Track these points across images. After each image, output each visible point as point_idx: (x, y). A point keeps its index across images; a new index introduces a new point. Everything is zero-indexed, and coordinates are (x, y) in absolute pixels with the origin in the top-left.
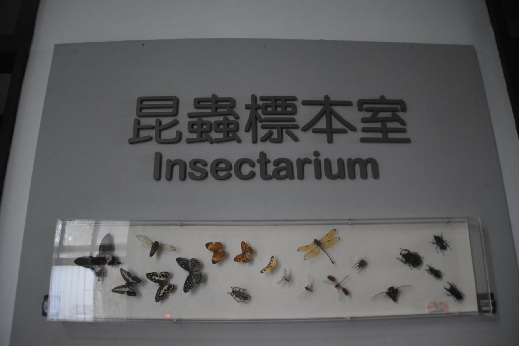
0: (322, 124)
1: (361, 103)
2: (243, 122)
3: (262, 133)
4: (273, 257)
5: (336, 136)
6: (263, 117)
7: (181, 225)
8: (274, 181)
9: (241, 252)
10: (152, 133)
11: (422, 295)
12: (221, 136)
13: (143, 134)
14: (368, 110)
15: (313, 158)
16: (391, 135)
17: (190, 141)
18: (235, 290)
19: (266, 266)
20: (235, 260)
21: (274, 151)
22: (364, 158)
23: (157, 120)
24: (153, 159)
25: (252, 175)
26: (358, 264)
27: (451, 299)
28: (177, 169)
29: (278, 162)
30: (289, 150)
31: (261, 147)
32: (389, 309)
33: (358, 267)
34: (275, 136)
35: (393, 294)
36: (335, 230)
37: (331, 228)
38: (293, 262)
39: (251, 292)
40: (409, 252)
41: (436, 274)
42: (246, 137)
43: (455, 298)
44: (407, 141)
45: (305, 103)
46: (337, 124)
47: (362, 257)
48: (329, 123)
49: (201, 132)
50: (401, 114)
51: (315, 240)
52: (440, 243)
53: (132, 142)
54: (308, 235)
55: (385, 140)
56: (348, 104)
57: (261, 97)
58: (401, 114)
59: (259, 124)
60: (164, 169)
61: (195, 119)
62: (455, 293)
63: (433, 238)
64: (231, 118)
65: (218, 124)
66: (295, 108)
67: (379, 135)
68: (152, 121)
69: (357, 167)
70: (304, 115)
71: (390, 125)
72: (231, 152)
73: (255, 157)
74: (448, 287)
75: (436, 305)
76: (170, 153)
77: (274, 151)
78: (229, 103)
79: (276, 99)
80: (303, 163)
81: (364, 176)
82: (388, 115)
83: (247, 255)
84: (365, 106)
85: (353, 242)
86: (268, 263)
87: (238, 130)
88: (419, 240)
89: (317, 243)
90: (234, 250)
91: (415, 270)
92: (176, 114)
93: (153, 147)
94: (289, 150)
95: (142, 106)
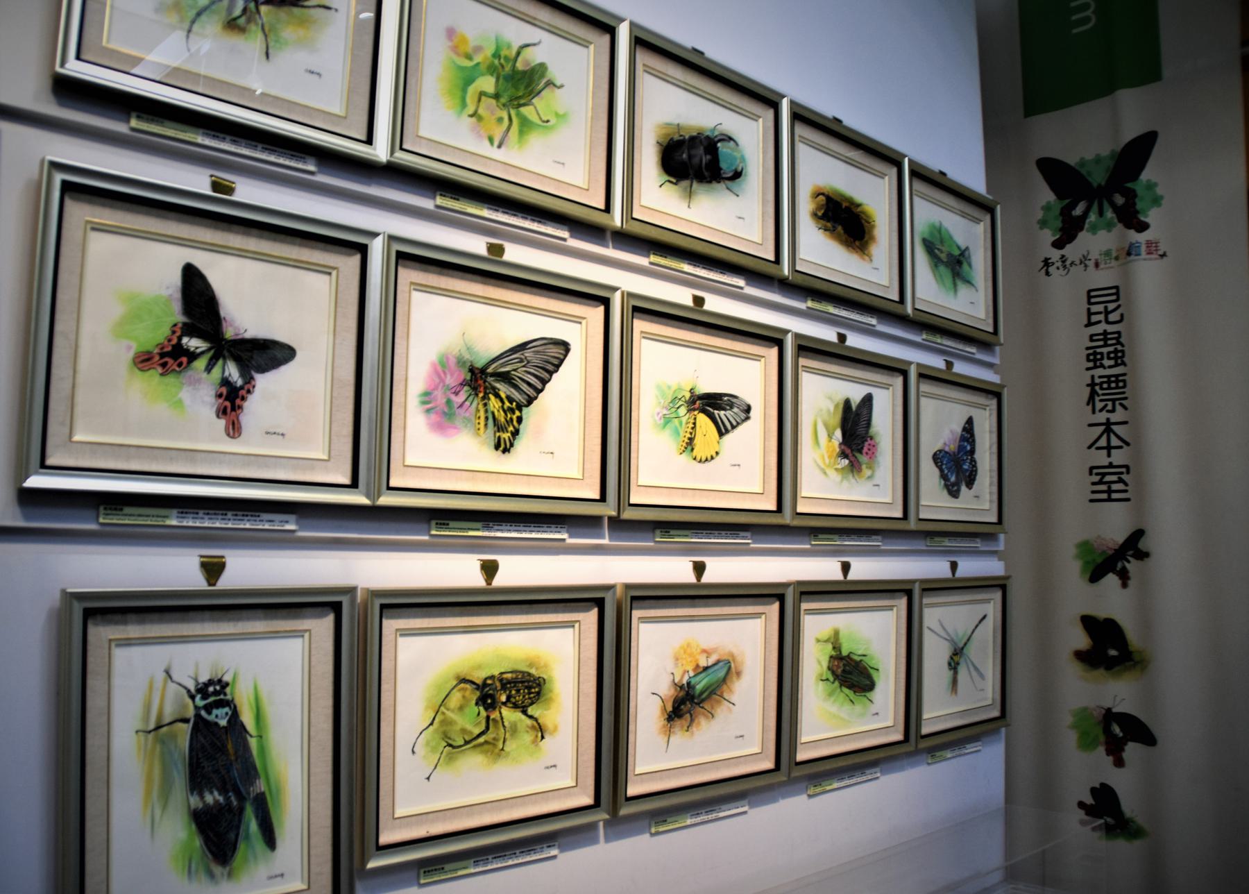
0: (1103, 442)
3: (1099, 405)
5: (1113, 452)
6: (1100, 392)
10: (1101, 317)
12: (1112, 362)
13: (1094, 318)
16: (1114, 496)
34: (1110, 407)
44: (1128, 500)
46: (1115, 442)
55: (1109, 500)
59: (1097, 399)
64: (1119, 347)
65: (1109, 353)
67: (1105, 496)
68: (1100, 308)
71: (1114, 487)
82: (1114, 478)
84: (1095, 471)
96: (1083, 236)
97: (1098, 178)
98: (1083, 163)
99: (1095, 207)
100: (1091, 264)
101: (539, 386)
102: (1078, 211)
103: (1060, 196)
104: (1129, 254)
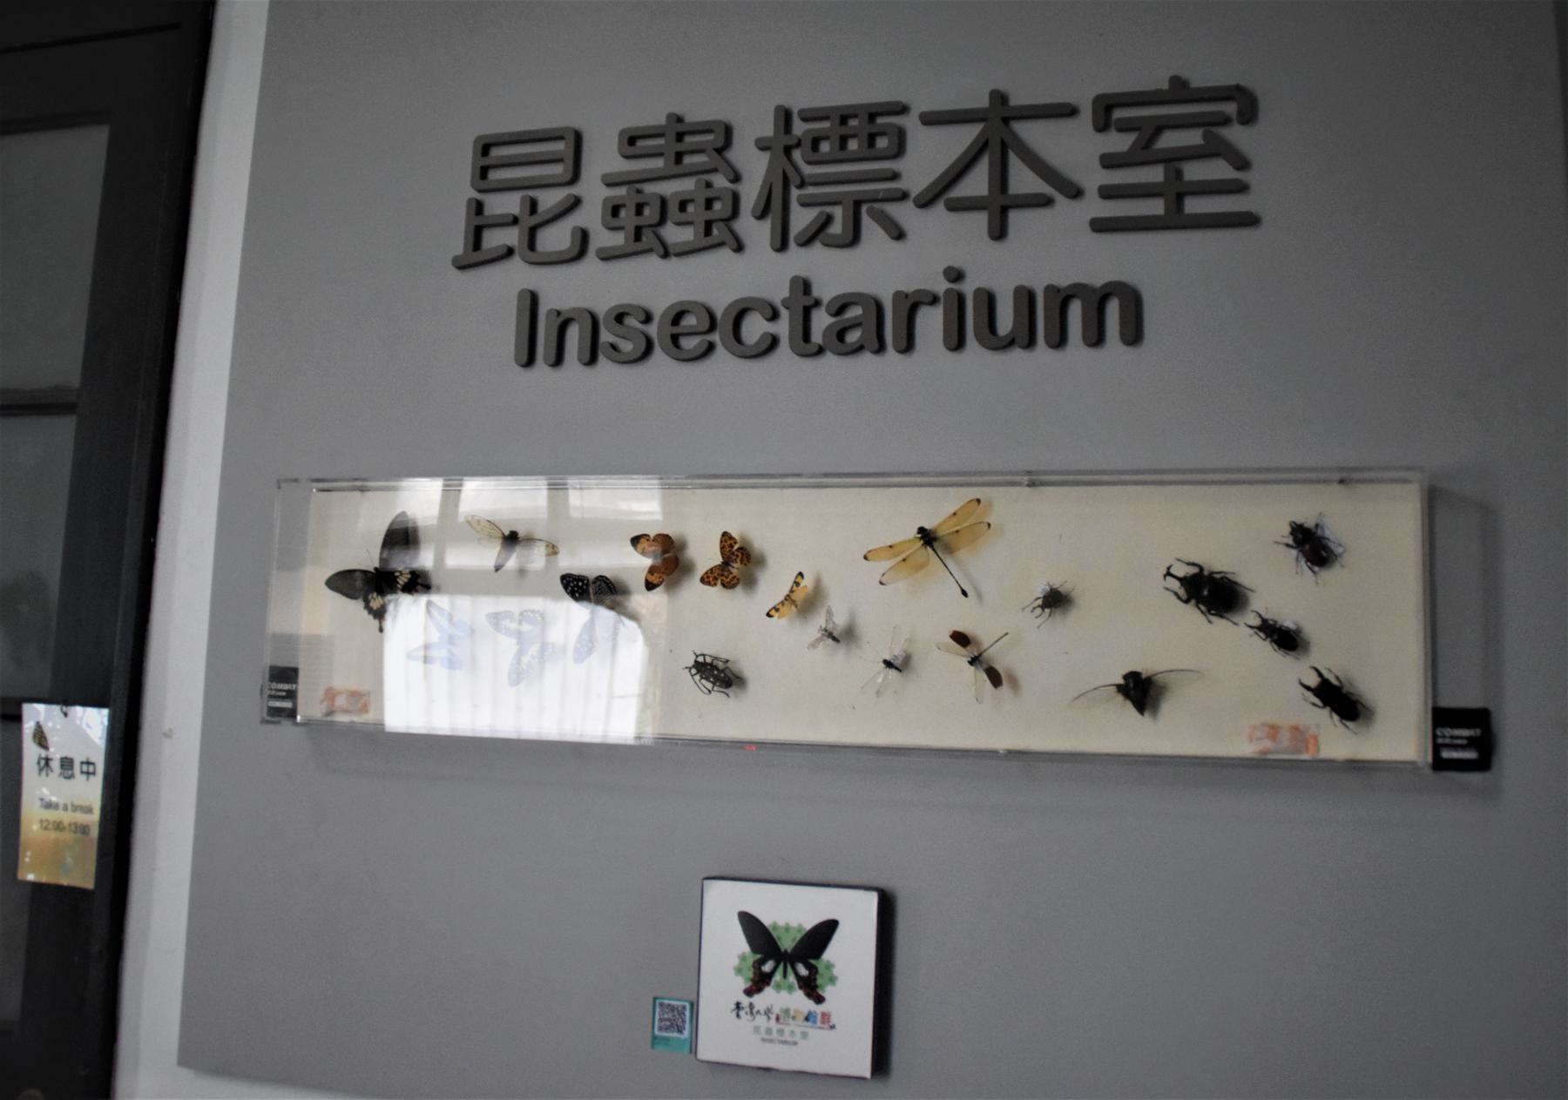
0: (977, 183)
1: (1106, 111)
2: (750, 192)
3: (802, 218)
4: (801, 574)
5: (1018, 219)
7: (1032, 484)
8: (830, 361)
9: (718, 560)
11: (1233, 697)
14: (1125, 127)
15: (941, 286)
16: (1193, 206)
17: (608, 256)
18: (701, 659)
19: (782, 598)
20: (702, 580)
21: (834, 272)
22: (1098, 279)
23: (523, 199)
24: (514, 312)
25: (771, 344)
26: (1040, 602)
27: (1323, 721)
28: (575, 338)
29: (840, 308)
30: (873, 269)
31: (800, 261)
32: (1128, 733)
33: (1039, 610)
35: (1140, 691)
36: (978, 501)
37: (974, 493)
38: (854, 591)
39: (746, 666)
40: (1201, 568)
41: (1286, 639)
42: (756, 231)
43: (1336, 717)
44: (1248, 220)
45: (931, 119)
47: (1057, 579)
48: (1001, 177)
49: (643, 227)
50: (1235, 134)
51: (921, 530)
52: (1312, 546)
53: (462, 265)
54: (901, 513)
55: (1175, 221)
56: (1069, 111)
57: (801, 112)
58: (1235, 134)
59: (795, 193)
60: (542, 337)
61: (621, 191)
62: (1340, 700)
63: (1288, 529)
66: (900, 137)
67: (1155, 207)
69: (1075, 310)
70: (928, 155)
71: (1195, 172)
72: (716, 279)
73: (779, 292)
74: (1313, 681)
75: (1273, 731)
76: (567, 289)
77: (834, 272)
78: (710, 137)
79: (844, 116)
80: (911, 305)
81: (1096, 337)
82: (1193, 138)
83: (736, 568)
84: (1118, 114)
85: (1037, 534)
86: (786, 592)
87: (735, 213)
88: (1241, 534)
89: (927, 537)
90: (705, 555)
91: (1220, 625)
92: (575, 178)
93: (516, 276)
94: (873, 269)
95: (486, 161)
96: (769, 991)
97: (787, 944)
98: (775, 926)
99: (781, 968)
100: (773, 1017)
101: (287, 705)
102: (767, 968)
103: (754, 949)
104: (807, 1019)
